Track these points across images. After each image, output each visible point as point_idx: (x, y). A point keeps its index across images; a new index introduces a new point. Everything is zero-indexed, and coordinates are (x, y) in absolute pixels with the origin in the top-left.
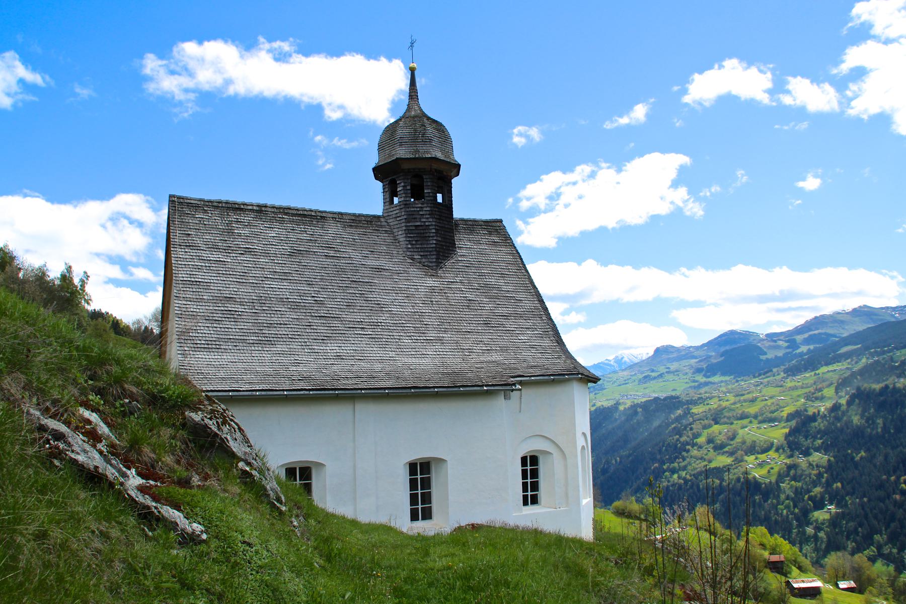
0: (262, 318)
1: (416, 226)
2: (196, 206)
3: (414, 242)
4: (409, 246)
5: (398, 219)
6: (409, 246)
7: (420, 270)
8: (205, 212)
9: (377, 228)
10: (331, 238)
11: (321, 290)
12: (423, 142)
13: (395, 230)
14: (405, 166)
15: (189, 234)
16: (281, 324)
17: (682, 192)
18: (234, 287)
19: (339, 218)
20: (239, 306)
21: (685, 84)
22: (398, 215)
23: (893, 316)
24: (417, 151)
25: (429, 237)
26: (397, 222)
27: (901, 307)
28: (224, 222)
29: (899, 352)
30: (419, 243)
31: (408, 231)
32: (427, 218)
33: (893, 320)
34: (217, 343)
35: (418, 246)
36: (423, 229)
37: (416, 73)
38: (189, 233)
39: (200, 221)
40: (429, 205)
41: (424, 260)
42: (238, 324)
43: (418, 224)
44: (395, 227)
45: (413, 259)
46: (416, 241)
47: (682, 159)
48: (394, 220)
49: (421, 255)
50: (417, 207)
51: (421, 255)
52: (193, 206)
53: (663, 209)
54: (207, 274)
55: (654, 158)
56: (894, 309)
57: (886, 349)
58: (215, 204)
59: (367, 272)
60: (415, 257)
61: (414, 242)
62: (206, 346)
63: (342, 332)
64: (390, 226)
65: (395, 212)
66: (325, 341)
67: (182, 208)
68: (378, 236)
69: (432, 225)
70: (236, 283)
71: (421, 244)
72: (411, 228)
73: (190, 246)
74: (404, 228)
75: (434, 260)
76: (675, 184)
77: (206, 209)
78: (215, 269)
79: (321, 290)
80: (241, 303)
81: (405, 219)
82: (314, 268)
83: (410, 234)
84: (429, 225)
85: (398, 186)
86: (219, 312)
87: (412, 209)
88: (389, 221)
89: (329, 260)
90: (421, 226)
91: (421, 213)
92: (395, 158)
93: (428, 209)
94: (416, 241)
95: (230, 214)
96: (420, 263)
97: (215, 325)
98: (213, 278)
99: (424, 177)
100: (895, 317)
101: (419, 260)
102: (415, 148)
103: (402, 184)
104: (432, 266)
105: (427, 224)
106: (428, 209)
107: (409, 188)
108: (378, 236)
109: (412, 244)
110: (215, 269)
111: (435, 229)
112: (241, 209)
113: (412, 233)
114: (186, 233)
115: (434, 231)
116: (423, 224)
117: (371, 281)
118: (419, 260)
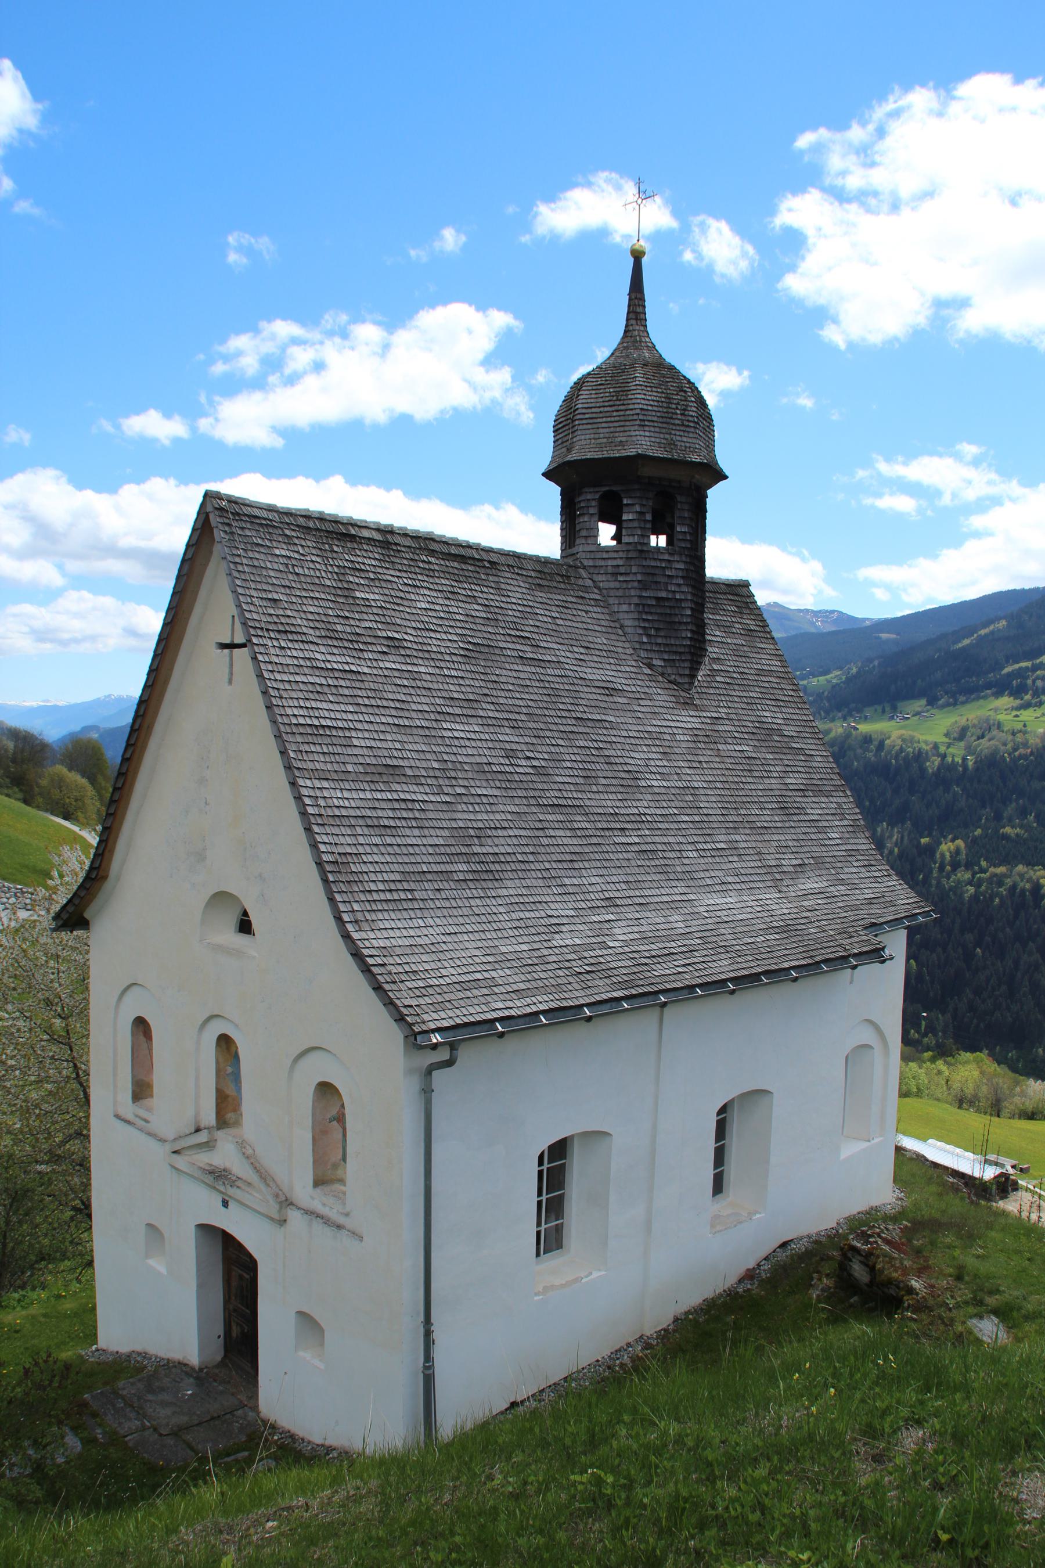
0: (463, 817)
1: (658, 599)
2: (267, 525)
3: (653, 632)
4: (645, 640)
5: (621, 578)
6: (645, 640)
7: (666, 692)
8: (289, 541)
9: (581, 594)
10: (518, 614)
11: (534, 741)
12: (683, 425)
13: (611, 601)
14: (647, 471)
15: (275, 600)
16: (496, 828)
17: (503, 376)
18: (391, 741)
19: (518, 568)
20: (415, 788)
21: (779, 278)
22: (622, 570)
23: (813, 624)
24: (672, 444)
25: (680, 623)
26: (617, 585)
27: (827, 611)
28: (330, 569)
29: (816, 679)
30: (662, 633)
31: (642, 608)
32: (679, 585)
33: (813, 630)
34: (406, 886)
35: (659, 641)
36: (670, 607)
37: (645, 260)
38: (276, 597)
39: (287, 565)
40: (684, 559)
41: (669, 670)
42: (426, 832)
43: (664, 594)
44: (612, 593)
45: (650, 666)
46: (657, 629)
47: (501, 319)
48: (609, 577)
49: (664, 660)
50: (660, 560)
51: (664, 660)
52: (261, 525)
53: (461, 397)
54: (336, 707)
55: (460, 313)
56: (816, 614)
57: (798, 673)
58: (302, 521)
59: (589, 695)
60: (655, 662)
61: (653, 632)
62: (389, 896)
63: (594, 840)
64: (599, 588)
65: (615, 563)
66: (576, 865)
67: (243, 528)
68: (587, 612)
69: (687, 600)
70: (395, 729)
71: (666, 637)
72: (649, 602)
73: (286, 632)
74: (636, 600)
75: (687, 672)
76: (489, 362)
77: (288, 532)
78: (346, 692)
79: (534, 741)
80: (416, 780)
81: (639, 581)
82: (511, 688)
83: (646, 613)
84: (681, 600)
85: (625, 509)
86: (383, 805)
87: (653, 563)
88: (596, 578)
89: (528, 669)
90: (667, 599)
91: (668, 573)
92: (632, 452)
93: (681, 566)
94: (657, 629)
95: (335, 548)
96: (662, 675)
97: (389, 840)
98: (350, 716)
99: (679, 498)
100: (816, 627)
101: (660, 669)
102: (667, 436)
103: (638, 508)
104: (682, 684)
105: (678, 597)
106: (681, 566)
107: (649, 517)
108: (587, 612)
109: (649, 636)
110: (346, 692)
111: (692, 609)
112: (352, 538)
113: (651, 613)
114: (270, 596)
115: (689, 612)
116: (670, 596)
117: (604, 717)
118: (660, 669)
